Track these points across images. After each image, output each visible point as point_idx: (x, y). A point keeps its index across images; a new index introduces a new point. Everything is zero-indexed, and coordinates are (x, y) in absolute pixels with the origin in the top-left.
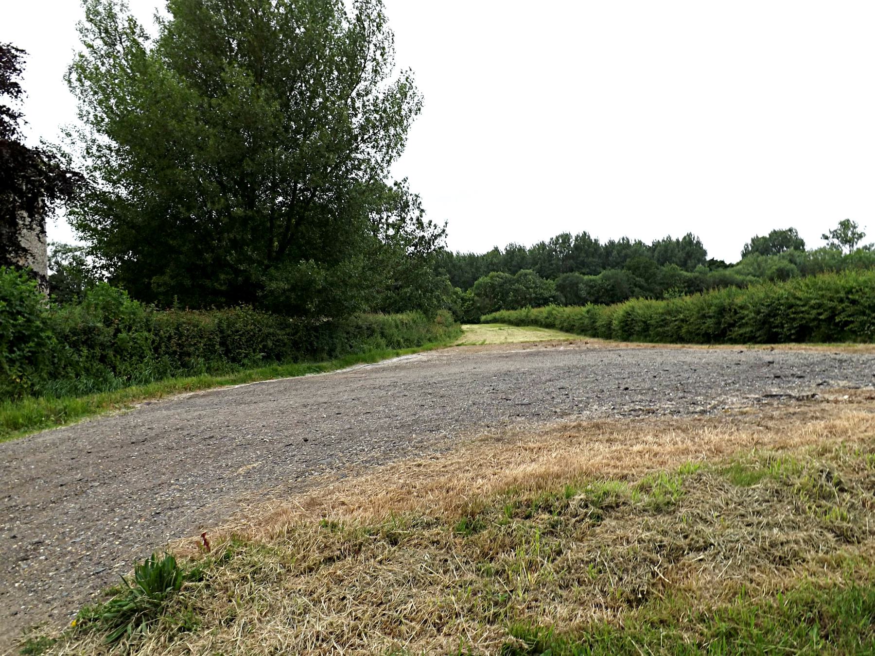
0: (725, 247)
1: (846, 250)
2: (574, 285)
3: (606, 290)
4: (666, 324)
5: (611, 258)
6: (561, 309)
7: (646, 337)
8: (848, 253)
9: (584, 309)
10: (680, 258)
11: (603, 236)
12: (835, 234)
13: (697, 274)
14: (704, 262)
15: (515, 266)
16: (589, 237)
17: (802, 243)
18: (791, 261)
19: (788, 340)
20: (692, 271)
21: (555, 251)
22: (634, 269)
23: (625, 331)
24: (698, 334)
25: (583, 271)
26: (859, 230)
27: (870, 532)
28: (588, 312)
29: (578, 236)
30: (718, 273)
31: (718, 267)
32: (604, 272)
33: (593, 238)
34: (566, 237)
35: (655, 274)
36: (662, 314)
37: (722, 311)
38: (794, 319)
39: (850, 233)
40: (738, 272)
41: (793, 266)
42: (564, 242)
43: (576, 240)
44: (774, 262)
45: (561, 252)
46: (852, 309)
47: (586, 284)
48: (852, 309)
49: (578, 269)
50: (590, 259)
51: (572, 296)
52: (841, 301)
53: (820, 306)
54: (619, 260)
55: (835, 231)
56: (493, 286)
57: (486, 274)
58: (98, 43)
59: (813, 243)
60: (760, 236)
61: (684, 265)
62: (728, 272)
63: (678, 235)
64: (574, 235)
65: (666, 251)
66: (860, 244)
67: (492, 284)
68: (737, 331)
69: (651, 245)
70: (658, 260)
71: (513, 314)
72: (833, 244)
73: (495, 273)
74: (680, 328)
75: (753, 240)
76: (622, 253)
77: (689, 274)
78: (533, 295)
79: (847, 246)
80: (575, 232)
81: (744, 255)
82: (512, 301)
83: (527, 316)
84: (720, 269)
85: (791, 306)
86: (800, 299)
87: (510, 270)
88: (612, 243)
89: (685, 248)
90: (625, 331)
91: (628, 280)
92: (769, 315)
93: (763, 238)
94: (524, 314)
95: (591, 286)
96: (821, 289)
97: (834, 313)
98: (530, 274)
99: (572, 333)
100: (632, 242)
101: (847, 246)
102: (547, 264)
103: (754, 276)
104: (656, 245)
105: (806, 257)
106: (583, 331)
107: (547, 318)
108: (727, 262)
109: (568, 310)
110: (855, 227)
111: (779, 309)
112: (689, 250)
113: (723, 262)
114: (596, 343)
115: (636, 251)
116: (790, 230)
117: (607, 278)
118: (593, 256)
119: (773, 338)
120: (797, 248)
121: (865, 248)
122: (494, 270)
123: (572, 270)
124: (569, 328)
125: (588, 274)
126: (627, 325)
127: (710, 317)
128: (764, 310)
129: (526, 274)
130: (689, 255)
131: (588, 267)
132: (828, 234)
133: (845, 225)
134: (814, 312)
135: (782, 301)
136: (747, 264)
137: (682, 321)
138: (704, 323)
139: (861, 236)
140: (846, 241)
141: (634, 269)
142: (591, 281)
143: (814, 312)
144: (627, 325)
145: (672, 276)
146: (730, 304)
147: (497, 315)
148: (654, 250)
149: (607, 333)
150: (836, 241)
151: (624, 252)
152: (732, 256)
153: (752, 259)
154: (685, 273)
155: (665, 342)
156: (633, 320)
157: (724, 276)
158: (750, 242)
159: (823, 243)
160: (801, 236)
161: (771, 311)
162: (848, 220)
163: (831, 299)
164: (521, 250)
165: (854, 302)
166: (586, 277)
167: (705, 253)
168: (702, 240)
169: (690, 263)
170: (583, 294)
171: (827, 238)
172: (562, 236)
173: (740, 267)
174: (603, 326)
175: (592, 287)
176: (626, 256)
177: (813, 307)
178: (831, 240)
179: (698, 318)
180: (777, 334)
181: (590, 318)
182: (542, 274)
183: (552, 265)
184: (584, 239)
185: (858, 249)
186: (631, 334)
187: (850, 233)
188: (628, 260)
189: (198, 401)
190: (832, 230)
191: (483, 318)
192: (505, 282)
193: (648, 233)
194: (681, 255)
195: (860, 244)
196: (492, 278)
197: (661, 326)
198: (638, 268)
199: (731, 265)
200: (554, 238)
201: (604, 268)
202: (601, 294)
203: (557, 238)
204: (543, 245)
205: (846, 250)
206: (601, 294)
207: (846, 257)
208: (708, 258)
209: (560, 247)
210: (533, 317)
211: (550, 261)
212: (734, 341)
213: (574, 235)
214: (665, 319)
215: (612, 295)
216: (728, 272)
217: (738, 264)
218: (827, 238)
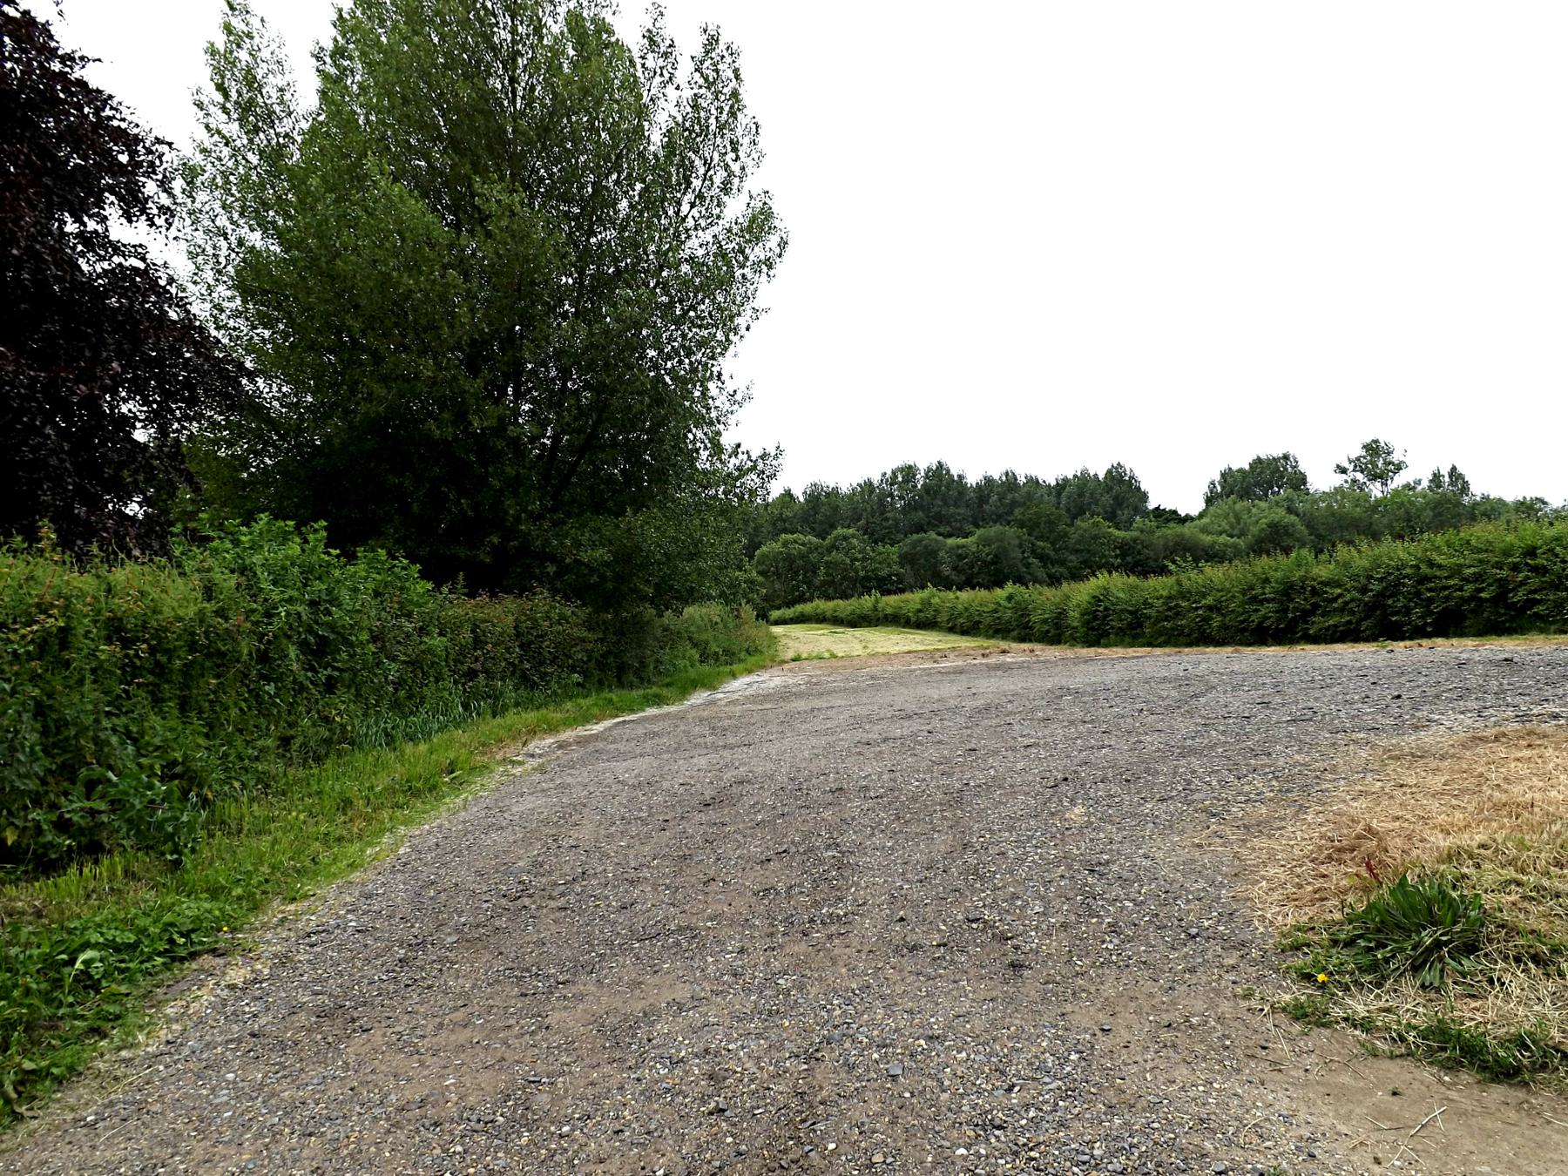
0: (1178, 488)
1: (1376, 490)
2: (932, 553)
3: (984, 562)
4: (1178, 614)
5: (986, 507)
6: (951, 595)
7: (1135, 637)
8: (1380, 495)
9: (1000, 594)
10: (1104, 507)
11: (973, 468)
12: (1358, 464)
13: (1135, 534)
14: (1146, 514)
15: (821, 522)
16: (948, 471)
17: (1303, 480)
18: (1290, 510)
19: (1419, 633)
20: (1128, 529)
21: (891, 495)
22: (1031, 526)
23: (1093, 629)
24: (1243, 630)
25: (941, 530)
26: (1396, 457)
27: (1359, 969)
28: (1010, 598)
29: (929, 470)
30: (1173, 530)
31: (1168, 521)
32: (979, 532)
33: (955, 472)
34: (909, 471)
35: (1066, 534)
36: (1170, 597)
37: (1288, 590)
38: (1430, 601)
39: (1380, 463)
40: (1204, 530)
41: (1293, 518)
42: (906, 481)
43: (927, 477)
44: (1265, 512)
45: (901, 498)
46: (1535, 581)
47: (951, 550)
48: (1535, 581)
49: (933, 527)
50: (952, 509)
51: (924, 570)
52: (1515, 568)
53: (1478, 578)
54: (1001, 511)
55: (1358, 459)
56: (789, 559)
57: (775, 535)
58: (233, 129)
59: (1322, 479)
60: (1235, 468)
61: (1111, 516)
62: (1186, 530)
63: (1099, 469)
64: (922, 466)
65: (1081, 495)
66: (1399, 481)
67: (789, 555)
68: (1318, 623)
69: (1053, 483)
70: (1068, 510)
71: (843, 606)
72: (1354, 481)
73: (789, 536)
74: (1206, 620)
75: (1223, 475)
76: (1005, 498)
77: (1121, 534)
78: (862, 574)
79: (1378, 485)
80: (924, 462)
81: (1209, 501)
82: (823, 583)
83: (875, 608)
84: (1172, 524)
85: (1425, 579)
86: (1440, 567)
87: (813, 529)
88: (989, 480)
89: (1111, 489)
90: (1093, 629)
91: (1020, 546)
92: (1381, 595)
93: (1240, 470)
94: (870, 605)
95: (959, 555)
96: (1480, 551)
97: (1504, 587)
98: (853, 536)
99: (974, 635)
100: (1022, 480)
101: (1378, 485)
102: (877, 519)
103: (1232, 536)
104: (1062, 485)
105: (1315, 502)
106: (997, 631)
107: (920, 611)
108: (1183, 513)
109: (965, 595)
110: (1389, 453)
111: (1404, 585)
112: (1120, 491)
113: (1175, 512)
114: (1018, 652)
115: (1029, 496)
116: (1286, 457)
117: (986, 542)
118: (956, 505)
119: (1389, 630)
120: (1296, 488)
121: (1408, 487)
122: (785, 531)
123: (920, 528)
124: (968, 626)
125: (950, 536)
126: (1095, 618)
127: (1268, 601)
128: (1376, 587)
129: (845, 538)
130: (1119, 502)
131: (948, 523)
132: (1345, 464)
133: (1373, 449)
134: (1469, 587)
135: (1408, 571)
136: (1217, 516)
137: (1210, 608)
138: (1257, 611)
139: (1399, 467)
140: (1380, 476)
141: (1031, 526)
142: (959, 547)
143: (1469, 587)
144: (1095, 618)
145: (1095, 538)
146: (1303, 579)
147: (807, 608)
148: (1059, 494)
149: (1055, 632)
150: (1360, 477)
151: (1009, 496)
152: (1191, 504)
153: (1225, 507)
154: (1117, 533)
155: (1176, 645)
156: (1106, 609)
157: (1182, 535)
158: (1217, 478)
159: (1339, 480)
160: (1302, 467)
161: (1386, 588)
162: (1376, 441)
163: (1499, 566)
164: (835, 493)
165: (1539, 570)
166: (951, 541)
167: (1144, 497)
168: (1137, 474)
169: (1123, 515)
170: (946, 570)
171: (1344, 471)
172: (902, 470)
173: (1205, 520)
174: (1045, 621)
175: (961, 557)
176: (1014, 504)
177: (1466, 580)
178: (1351, 475)
179: (1243, 603)
180: (1399, 625)
181: (1015, 609)
182: (875, 536)
183: (887, 519)
184: (939, 473)
185: (1396, 491)
186: (1106, 634)
187: (1380, 463)
188: (1017, 511)
189: (627, 731)
190: (1353, 457)
191: (775, 614)
192: (810, 551)
193: (1050, 460)
194: (1107, 499)
195: (1399, 481)
196: (785, 544)
197: (1167, 619)
198: (1037, 525)
199: (1188, 518)
200: (889, 474)
201: (978, 527)
202: (976, 570)
203: (894, 473)
204: (869, 485)
205: (1376, 490)
206: (976, 570)
207: (1378, 502)
208: (1151, 505)
209: (900, 488)
210: (889, 611)
211: (882, 513)
212: (1315, 640)
213: (922, 466)
214: (1177, 606)
215: (991, 572)
216: (1186, 530)
217: (1201, 515)
218: (1344, 471)
